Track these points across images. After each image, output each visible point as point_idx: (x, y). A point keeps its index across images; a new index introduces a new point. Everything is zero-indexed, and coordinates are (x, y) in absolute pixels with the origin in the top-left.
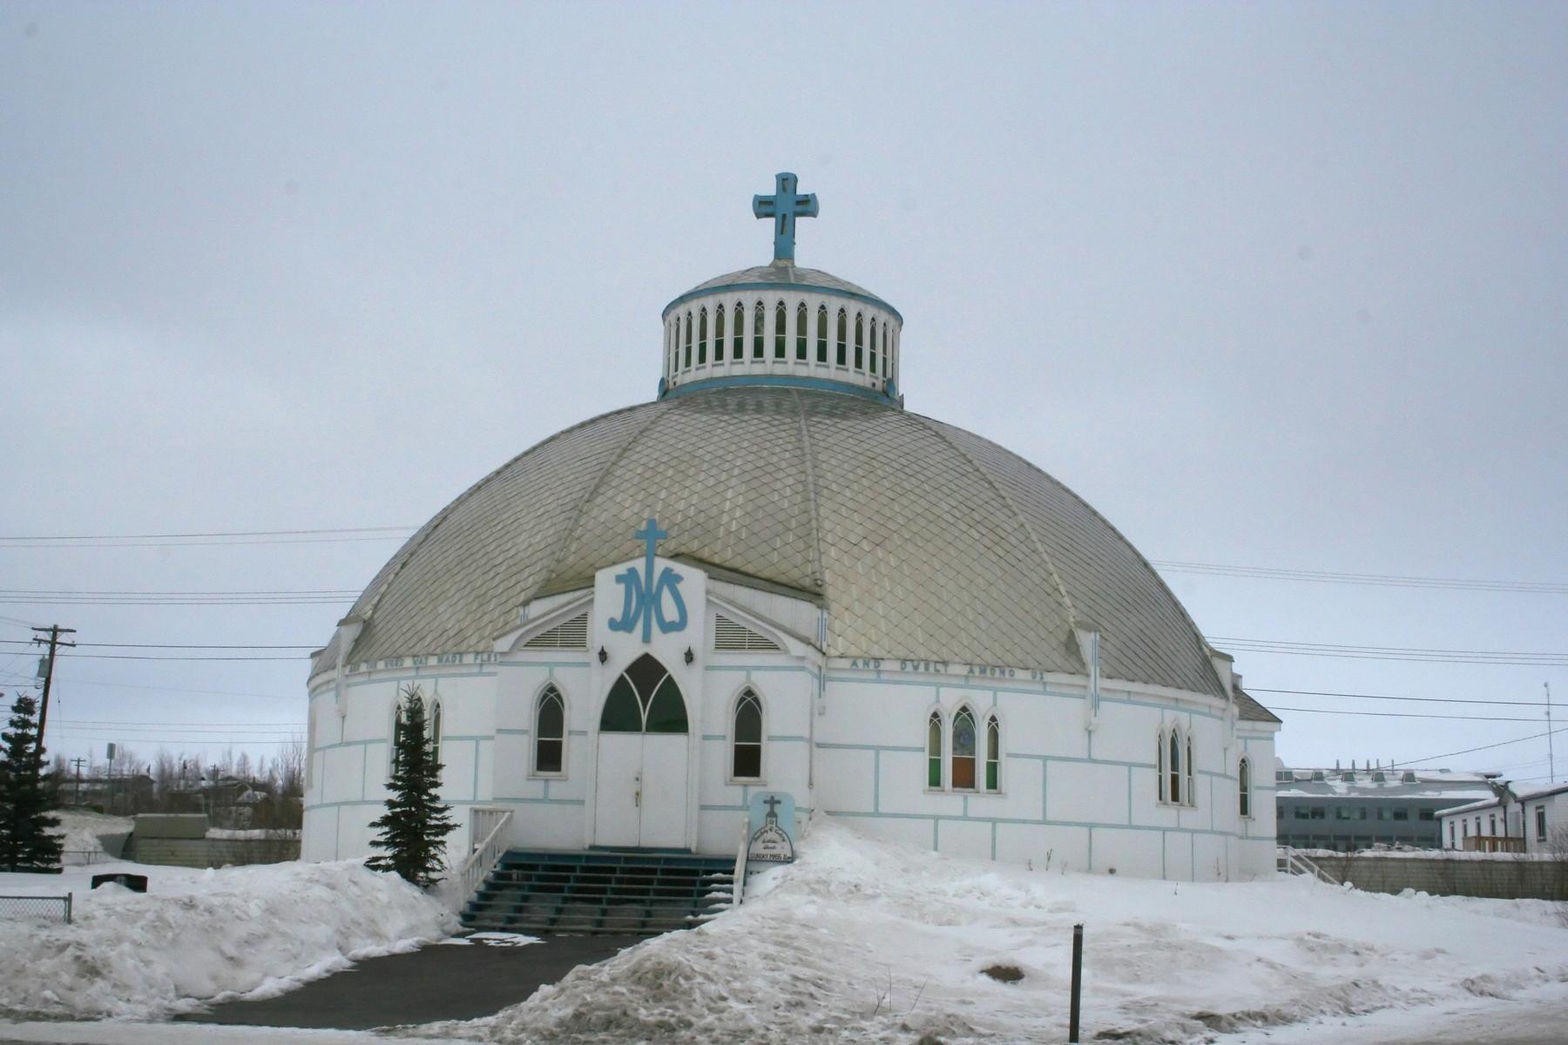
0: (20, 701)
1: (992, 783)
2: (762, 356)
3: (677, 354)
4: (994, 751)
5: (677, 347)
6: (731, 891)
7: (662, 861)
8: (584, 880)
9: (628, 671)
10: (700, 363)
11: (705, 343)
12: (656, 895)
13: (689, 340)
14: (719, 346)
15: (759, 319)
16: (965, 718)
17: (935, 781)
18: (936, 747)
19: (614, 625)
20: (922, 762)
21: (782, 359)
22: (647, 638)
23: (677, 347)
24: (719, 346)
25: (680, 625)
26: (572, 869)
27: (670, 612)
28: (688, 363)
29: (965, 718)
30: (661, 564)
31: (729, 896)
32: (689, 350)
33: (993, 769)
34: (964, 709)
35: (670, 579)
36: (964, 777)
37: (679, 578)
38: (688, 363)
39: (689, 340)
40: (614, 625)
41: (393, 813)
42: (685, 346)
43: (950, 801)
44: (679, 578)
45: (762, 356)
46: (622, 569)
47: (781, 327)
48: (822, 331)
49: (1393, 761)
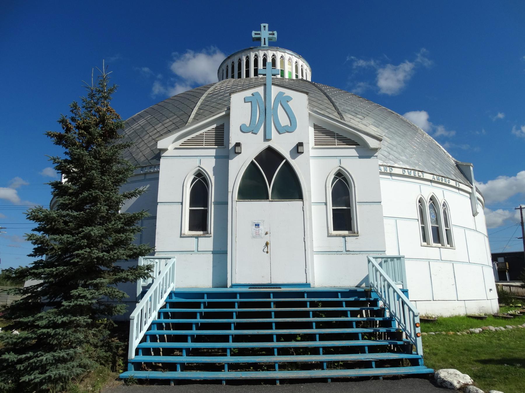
0: (337, 227)
1: (449, 241)
4: (447, 225)
6: (223, 138)
8: (203, 326)
9: (256, 159)
12: (276, 307)
19: (243, 130)
20: (417, 226)
22: (266, 139)
25: (290, 129)
26: (197, 305)
27: (284, 121)
30: (275, 91)
31: (223, 131)
33: (448, 232)
35: (283, 101)
37: (289, 99)
40: (243, 130)
41: (38, 247)
44: (289, 99)
46: (248, 93)
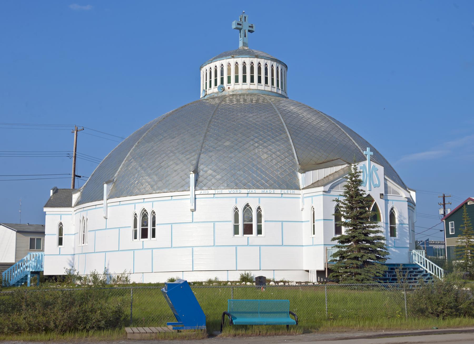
2: (238, 82)
3: (206, 83)
5: (206, 80)
7: (396, 265)
10: (215, 86)
11: (210, 79)
13: (211, 78)
14: (229, 78)
15: (229, 70)
16: (247, 208)
17: (236, 232)
18: (135, 226)
21: (253, 83)
23: (206, 80)
24: (229, 78)
28: (210, 87)
29: (247, 208)
32: (210, 82)
33: (154, 231)
34: (247, 205)
36: (248, 230)
38: (210, 87)
39: (211, 78)
42: (214, 78)
43: (242, 238)
45: (238, 82)
47: (266, 73)
48: (237, 71)
49: (444, 195)
